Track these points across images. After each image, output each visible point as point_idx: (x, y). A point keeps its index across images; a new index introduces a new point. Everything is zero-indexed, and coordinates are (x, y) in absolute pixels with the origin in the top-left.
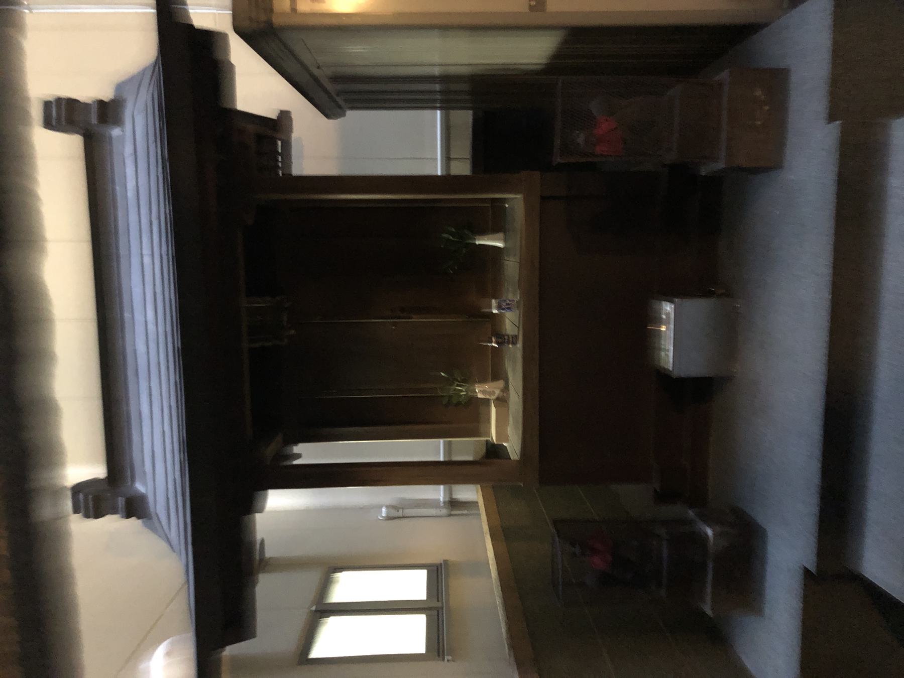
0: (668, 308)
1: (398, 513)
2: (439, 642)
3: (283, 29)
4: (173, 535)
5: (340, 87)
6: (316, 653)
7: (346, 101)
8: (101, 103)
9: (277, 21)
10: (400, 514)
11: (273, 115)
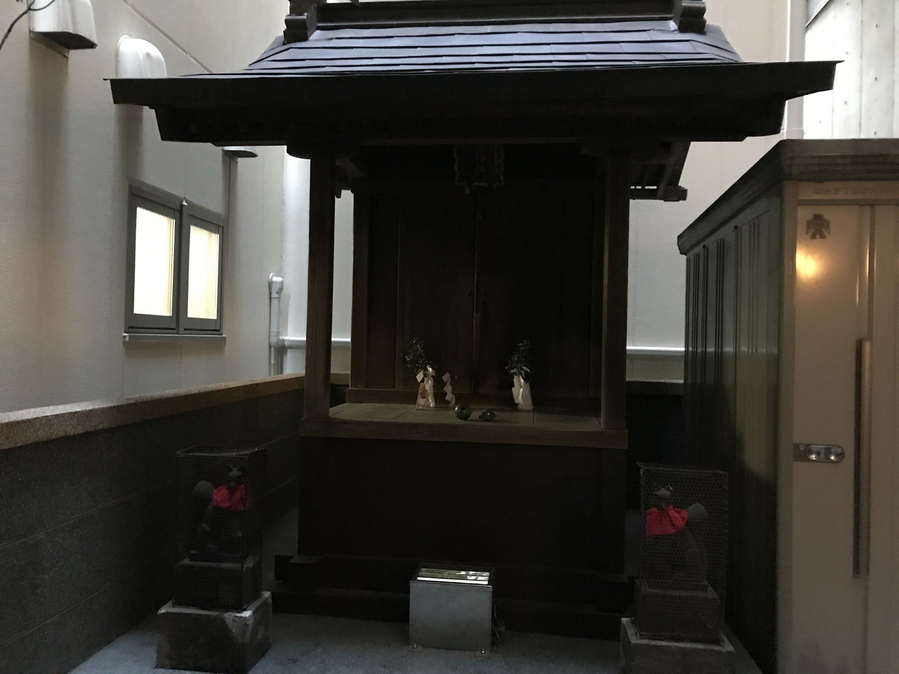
0: (483, 579)
1: (274, 293)
2: (140, 327)
3: (780, 193)
4: (266, 64)
5: (713, 248)
6: (143, 215)
7: (697, 256)
8: (702, 11)
9: (789, 188)
10: (274, 295)
11: (682, 183)
